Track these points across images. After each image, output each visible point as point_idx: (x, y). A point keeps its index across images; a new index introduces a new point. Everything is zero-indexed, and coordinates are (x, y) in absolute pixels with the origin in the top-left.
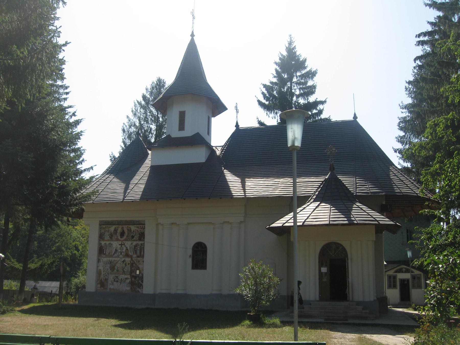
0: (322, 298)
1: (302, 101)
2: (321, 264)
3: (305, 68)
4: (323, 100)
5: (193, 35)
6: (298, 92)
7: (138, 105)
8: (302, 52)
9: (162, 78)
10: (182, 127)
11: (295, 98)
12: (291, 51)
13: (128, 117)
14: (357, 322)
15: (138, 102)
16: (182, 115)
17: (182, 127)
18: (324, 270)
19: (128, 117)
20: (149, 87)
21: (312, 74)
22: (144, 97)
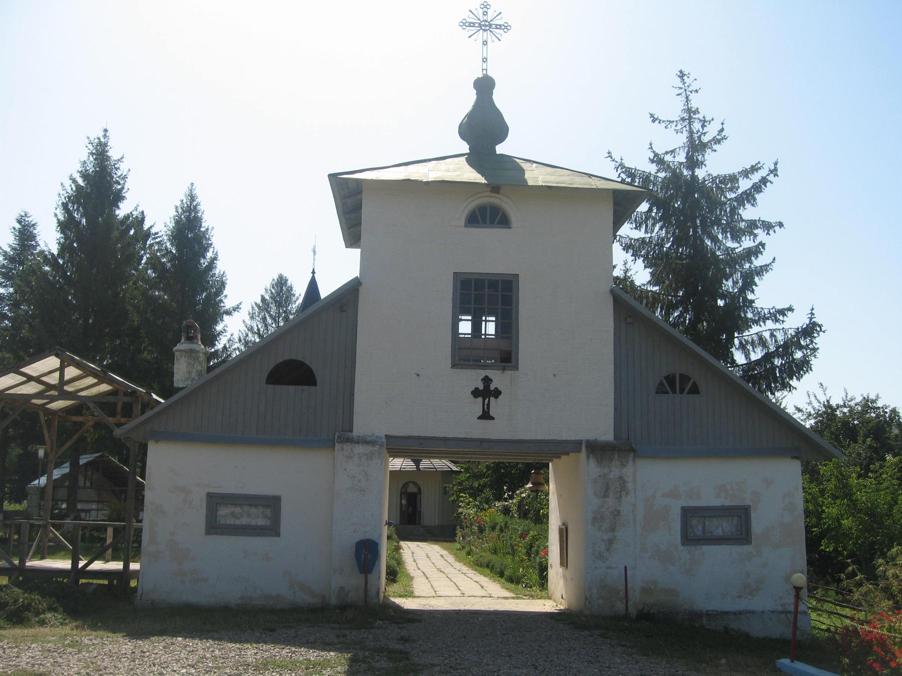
0: (401, 523)
5: (313, 272)
7: (256, 308)
9: (285, 274)
13: (244, 322)
15: (256, 304)
18: (404, 502)
19: (244, 322)
20: (268, 286)
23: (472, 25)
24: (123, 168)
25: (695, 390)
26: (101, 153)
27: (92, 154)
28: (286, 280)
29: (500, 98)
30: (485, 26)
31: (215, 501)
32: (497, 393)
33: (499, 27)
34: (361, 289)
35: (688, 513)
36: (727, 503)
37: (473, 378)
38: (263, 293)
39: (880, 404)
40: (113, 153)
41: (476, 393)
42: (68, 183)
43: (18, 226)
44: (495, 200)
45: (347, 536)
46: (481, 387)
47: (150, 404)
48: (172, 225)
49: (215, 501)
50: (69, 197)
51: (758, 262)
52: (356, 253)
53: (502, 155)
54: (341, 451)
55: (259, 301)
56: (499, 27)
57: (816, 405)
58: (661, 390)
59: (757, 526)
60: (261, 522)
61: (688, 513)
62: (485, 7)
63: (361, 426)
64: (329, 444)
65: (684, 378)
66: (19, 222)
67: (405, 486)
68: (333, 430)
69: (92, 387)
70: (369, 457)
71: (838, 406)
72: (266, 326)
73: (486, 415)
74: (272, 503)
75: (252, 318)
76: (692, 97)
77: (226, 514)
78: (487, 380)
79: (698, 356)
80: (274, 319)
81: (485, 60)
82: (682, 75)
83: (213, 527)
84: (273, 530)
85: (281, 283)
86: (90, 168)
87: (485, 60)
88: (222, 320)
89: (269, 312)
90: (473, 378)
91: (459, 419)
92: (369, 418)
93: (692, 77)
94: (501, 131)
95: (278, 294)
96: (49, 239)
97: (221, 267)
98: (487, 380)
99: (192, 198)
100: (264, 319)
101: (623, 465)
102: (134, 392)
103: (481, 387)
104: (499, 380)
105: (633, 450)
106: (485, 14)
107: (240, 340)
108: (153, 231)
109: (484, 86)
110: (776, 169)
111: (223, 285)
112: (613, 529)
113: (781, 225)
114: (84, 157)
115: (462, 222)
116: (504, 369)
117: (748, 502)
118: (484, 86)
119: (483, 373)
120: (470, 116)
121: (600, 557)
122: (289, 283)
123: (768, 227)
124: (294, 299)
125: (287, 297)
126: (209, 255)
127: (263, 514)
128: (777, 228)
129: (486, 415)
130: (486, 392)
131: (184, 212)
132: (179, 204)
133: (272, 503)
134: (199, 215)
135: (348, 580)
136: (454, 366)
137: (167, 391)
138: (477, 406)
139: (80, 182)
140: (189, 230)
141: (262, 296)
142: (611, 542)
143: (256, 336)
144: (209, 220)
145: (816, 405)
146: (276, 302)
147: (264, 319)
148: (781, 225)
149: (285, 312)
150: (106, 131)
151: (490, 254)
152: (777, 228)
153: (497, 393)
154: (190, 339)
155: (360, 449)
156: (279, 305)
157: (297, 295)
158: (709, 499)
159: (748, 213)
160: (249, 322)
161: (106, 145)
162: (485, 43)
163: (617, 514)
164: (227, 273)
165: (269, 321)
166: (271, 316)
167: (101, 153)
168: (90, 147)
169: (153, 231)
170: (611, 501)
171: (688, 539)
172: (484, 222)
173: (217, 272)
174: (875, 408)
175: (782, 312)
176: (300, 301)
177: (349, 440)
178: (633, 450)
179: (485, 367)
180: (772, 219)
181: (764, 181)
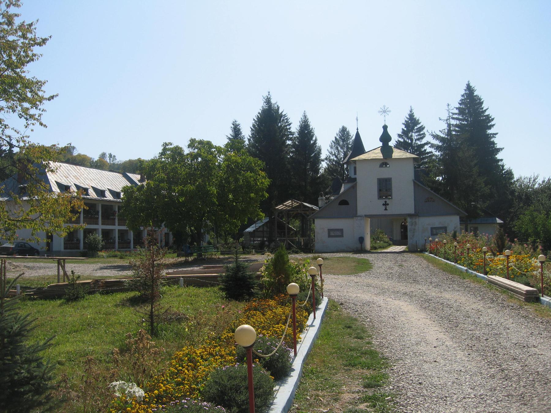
1: (419, 143)
2: (401, 228)
3: (420, 123)
4: (382, 130)
5: (357, 129)
6: (416, 138)
8: (416, 116)
11: (414, 141)
12: (411, 116)
14: (3, 271)
21: (422, 128)
30: (385, 112)
32: (388, 204)
37: (383, 201)
38: (336, 135)
41: (383, 205)
43: (233, 126)
48: (299, 128)
49: (330, 231)
55: (334, 140)
62: (384, 106)
63: (359, 213)
64: (352, 217)
65: (432, 199)
66: (233, 125)
68: (353, 214)
69: (295, 204)
73: (386, 209)
74: (341, 230)
75: (331, 148)
77: (332, 233)
78: (386, 202)
79: (205, 273)
80: (342, 148)
83: (330, 236)
84: (342, 236)
90: (383, 201)
91: (380, 210)
95: (343, 136)
96: (247, 133)
97: (319, 143)
98: (386, 202)
99: (305, 117)
104: (388, 201)
108: (283, 114)
109: (385, 128)
111: (320, 150)
114: (262, 105)
118: (385, 128)
119: (385, 200)
124: (350, 137)
126: (314, 139)
129: (386, 209)
130: (386, 204)
133: (341, 230)
135: (359, 245)
138: (384, 207)
140: (306, 131)
141: (336, 138)
144: (313, 125)
146: (342, 139)
147: (337, 148)
151: (385, 173)
153: (388, 204)
154: (321, 196)
155: (359, 218)
156: (343, 141)
158: (437, 225)
160: (330, 150)
163: (415, 229)
169: (283, 114)
176: (354, 138)
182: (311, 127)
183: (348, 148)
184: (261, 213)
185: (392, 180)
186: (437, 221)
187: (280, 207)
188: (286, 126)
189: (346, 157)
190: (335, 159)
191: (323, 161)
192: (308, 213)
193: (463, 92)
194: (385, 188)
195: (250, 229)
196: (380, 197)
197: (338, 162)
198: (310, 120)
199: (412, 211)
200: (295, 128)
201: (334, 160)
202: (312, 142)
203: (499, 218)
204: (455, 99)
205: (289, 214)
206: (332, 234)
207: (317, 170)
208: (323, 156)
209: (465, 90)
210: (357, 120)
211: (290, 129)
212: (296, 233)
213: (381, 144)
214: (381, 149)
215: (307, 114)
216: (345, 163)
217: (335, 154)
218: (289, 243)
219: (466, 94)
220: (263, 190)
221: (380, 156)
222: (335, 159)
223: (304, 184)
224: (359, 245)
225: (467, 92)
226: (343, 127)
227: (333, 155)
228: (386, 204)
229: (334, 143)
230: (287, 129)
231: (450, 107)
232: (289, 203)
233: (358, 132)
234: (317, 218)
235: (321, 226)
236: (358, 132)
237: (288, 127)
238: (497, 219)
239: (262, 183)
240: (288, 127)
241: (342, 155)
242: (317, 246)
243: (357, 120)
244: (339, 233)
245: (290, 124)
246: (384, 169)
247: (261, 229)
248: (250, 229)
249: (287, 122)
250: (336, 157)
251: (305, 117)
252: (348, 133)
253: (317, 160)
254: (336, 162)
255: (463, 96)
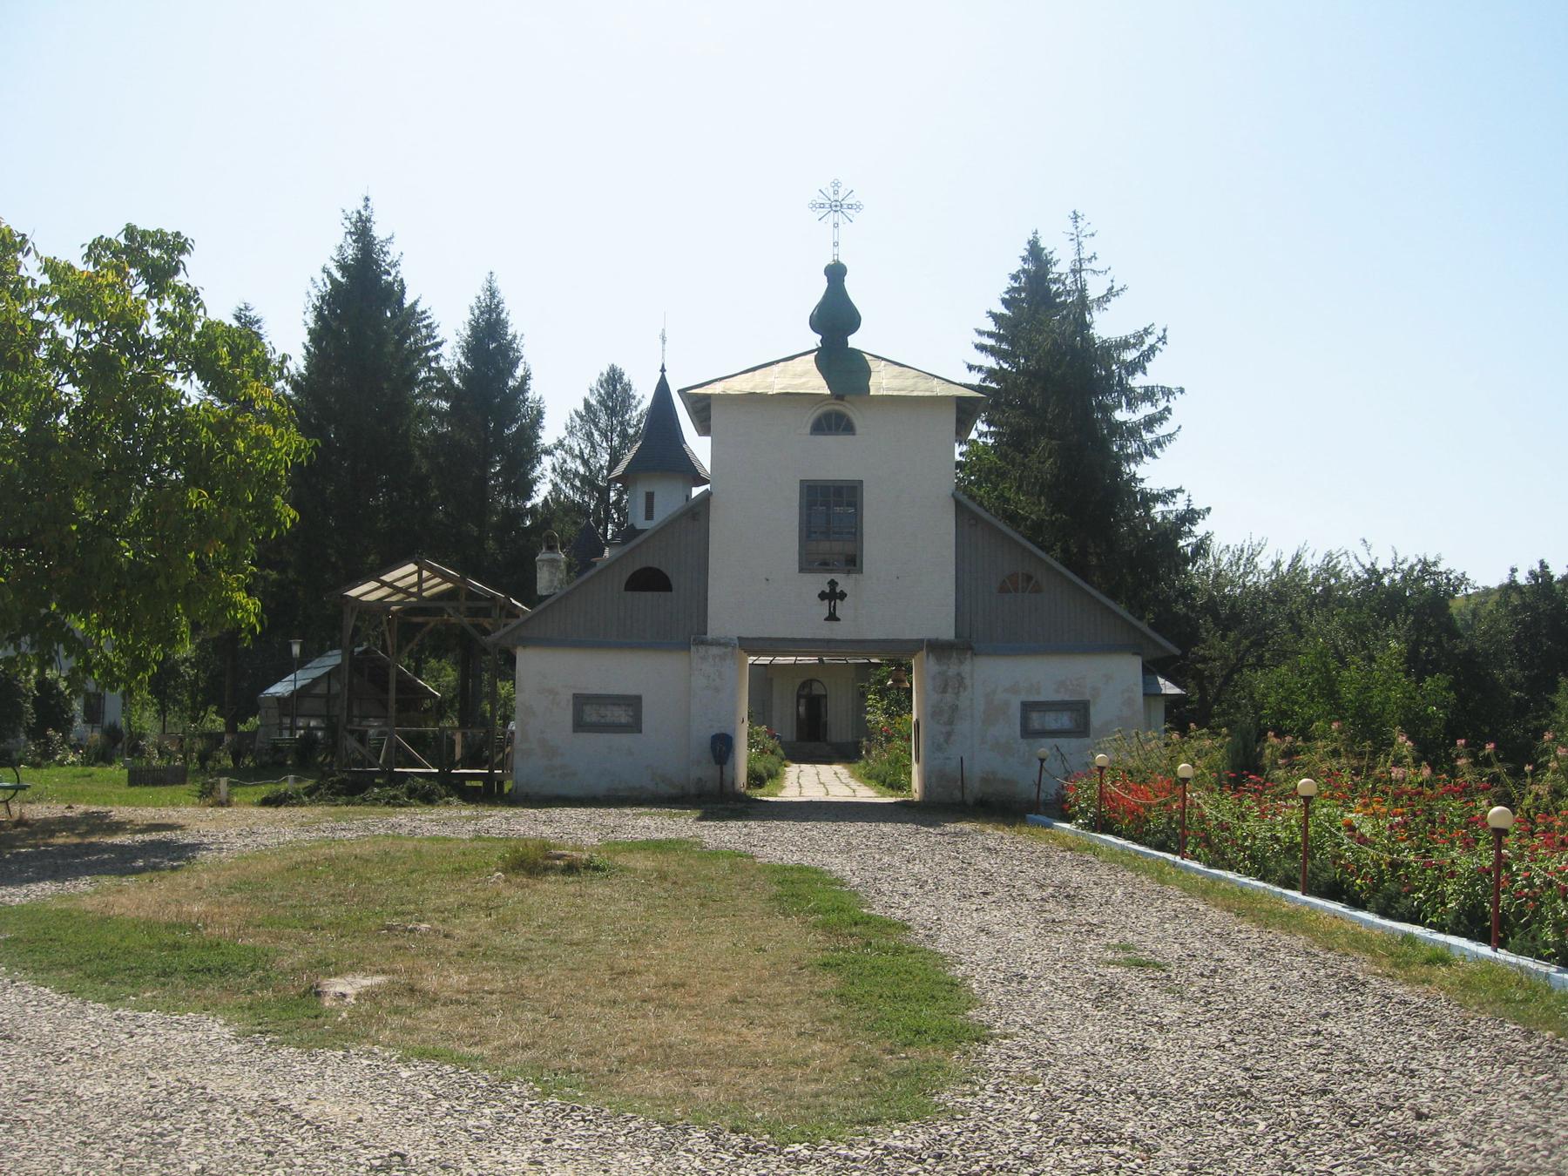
0: (799, 738)
4: (822, 285)
5: (663, 370)
9: (619, 366)
10: (649, 515)
16: (650, 497)
17: (649, 515)
18: (802, 709)
20: (595, 385)
22: (587, 405)
23: (822, 206)
24: (393, 252)
25: (1038, 590)
26: (362, 231)
27: (350, 233)
28: (621, 375)
29: (851, 285)
30: (836, 207)
31: (581, 701)
32: (843, 596)
33: (850, 207)
34: (712, 499)
35: (1028, 707)
36: (1067, 698)
37: (820, 582)
38: (587, 394)
39: (1442, 568)
40: (379, 232)
41: (823, 596)
42: (320, 277)
44: (838, 407)
45: (704, 731)
46: (828, 590)
47: (512, 613)
48: (466, 332)
49: (581, 701)
50: (323, 298)
51: (1161, 430)
52: (708, 439)
53: (853, 350)
54: (697, 652)
55: (581, 408)
56: (850, 207)
57: (1357, 569)
58: (1003, 590)
59: (1096, 719)
60: (624, 719)
61: (1028, 707)
62: (836, 184)
63: (715, 629)
64: (685, 646)
66: (238, 318)
67: (804, 685)
68: (688, 633)
69: (435, 586)
70: (723, 658)
71: (1386, 571)
72: (593, 446)
73: (832, 617)
76: (1086, 242)
77: (589, 713)
78: (833, 584)
80: (604, 435)
81: (836, 244)
82: (1076, 217)
83: (580, 725)
85: (614, 382)
86: (350, 252)
87: (836, 244)
88: (539, 462)
89: (596, 425)
90: (820, 582)
91: (809, 620)
92: (723, 619)
93: (1087, 219)
94: (851, 320)
95: (610, 395)
97: (535, 391)
98: (833, 584)
99: (492, 293)
100: (589, 436)
101: (961, 663)
102: (493, 597)
103: (828, 590)
104: (844, 583)
105: (971, 648)
106: (836, 193)
107: (554, 470)
109: (836, 273)
110: (1164, 337)
111: (540, 414)
112: (951, 722)
113: (1182, 391)
114: (340, 241)
115: (808, 430)
116: (849, 572)
117: (1087, 697)
118: (836, 273)
120: (822, 307)
121: (939, 748)
122: (625, 379)
123: (1167, 392)
124: (634, 403)
125: (623, 401)
126: (519, 372)
127: (624, 714)
128: (1178, 394)
129: (832, 617)
130: (832, 595)
131: (482, 313)
132: (473, 302)
134: (503, 316)
136: (801, 570)
137: (530, 598)
138: (824, 608)
139: (338, 275)
140: (490, 341)
142: (949, 735)
143: (578, 461)
144: (519, 323)
145: (1357, 569)
146: (607, 408)
147: (589, 436)
148: (1182, 391)
149: (621, 423)
150: (367, 199)
151: (835, 460)
152: (1178, 394)
153: (843, 596)
154: (551, 548)
155: (714, 650)
156: (612, 412)
157: (639, 396)
159: (1137, 382)
161: (368, 220)
162: (836, 225)
164: (545, 398)
165: (596, 435)
166: (599, 430)
167: (362, 231)
168: (347, 223)
170: (949, 697)
171: (1028, 732)
172: (830, 429)
173: (529, 395)
174: (1435, 573)
175: (1172, 493)
176: (646, 404)
177: (704, 643)
178: (971, 648)
179: (831, 571)
180: (1173, 385)
181: (1152, 349)
182: (510, 331)
183: (624, 435)
184: (240, 597)
185: (869, 497)
186: (1046, 676)
187: (366, 591)
188: (427, 349)
189: (617, 464)
190: (581, 470)
191: (548, 452)
192: (486, 623)
193: (1017, 265)
194: (831, 523)
195: (281, 688)
196: (809, 563)
197: (589, 482)
198: (507, 306)
199: (945, 630)
200: (450, 356)
201: (576, 474)
202: (511, 383)
203: (1168, 678)
204: (987, 290)
205: (412, 621)
206: (591, 715)
207: (526, 489)
208: (547, 437)
209: (1024, 259)
210: (664, 342)
211: (437, 358)
212: (440, 709)
213: (815, 340)
214: (817, 360)
215: (497, 284)
216: (617, 479)
217: (581, 456)
218: (399, 746)
219: (1024, 271)
220: (268, 482)
221: (816, 384)
222: (581, 470)
223: (475, 531)
224: (708, 771)
225: (1029, 266)
226: (613, 369)
227: (574, 457)
228: (832, 595)
229: (581, 417)
230: (429, 360)
231: (1081, 224)
232: (404, 574)
233: (663, 379)
234: (528, 642)
235: (545, 680)
236: (663, 379)
237: (432, 353)
238: (1161, 681)
239: (260, 442)
240: (432, 353)
241: (605, 458)
242: (525, 769)
243: (664, 342)
244: (621, 715)
245: (437, 345)
246: (832, 443)
247: (321, 689)
248: (281, 688)
249: (429, 337)
250: (585, 463)
251: (493, 295)
252: (627, 388)
253: (524, 450)
254: (583, 479)
255: (1015, 277)
